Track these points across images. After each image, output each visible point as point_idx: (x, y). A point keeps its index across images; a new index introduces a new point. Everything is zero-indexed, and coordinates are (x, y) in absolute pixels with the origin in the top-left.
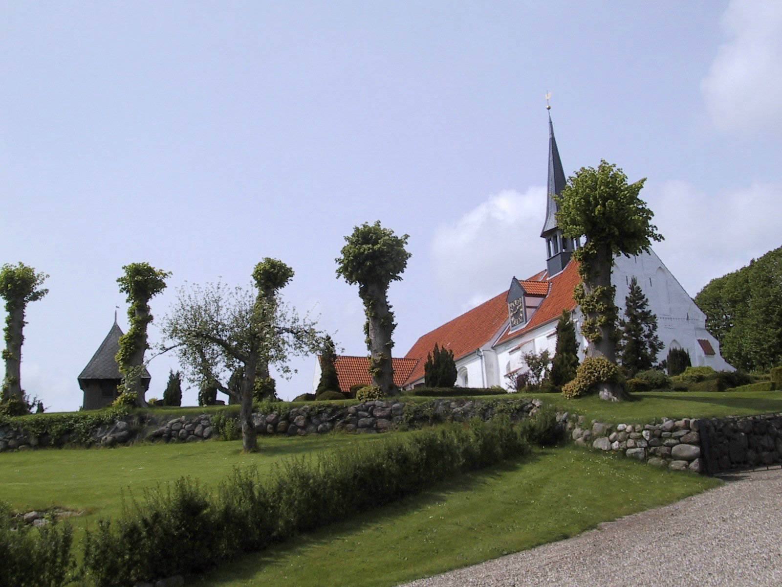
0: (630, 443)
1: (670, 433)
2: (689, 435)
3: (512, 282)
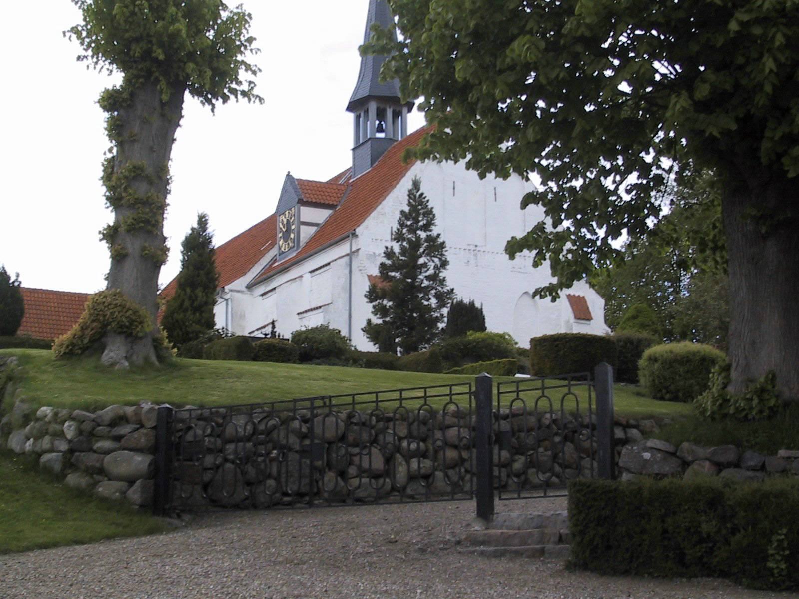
0: (46, 442)
1: (108, 429)
2: (136, 435)
3: (286, 182)
